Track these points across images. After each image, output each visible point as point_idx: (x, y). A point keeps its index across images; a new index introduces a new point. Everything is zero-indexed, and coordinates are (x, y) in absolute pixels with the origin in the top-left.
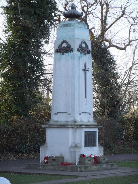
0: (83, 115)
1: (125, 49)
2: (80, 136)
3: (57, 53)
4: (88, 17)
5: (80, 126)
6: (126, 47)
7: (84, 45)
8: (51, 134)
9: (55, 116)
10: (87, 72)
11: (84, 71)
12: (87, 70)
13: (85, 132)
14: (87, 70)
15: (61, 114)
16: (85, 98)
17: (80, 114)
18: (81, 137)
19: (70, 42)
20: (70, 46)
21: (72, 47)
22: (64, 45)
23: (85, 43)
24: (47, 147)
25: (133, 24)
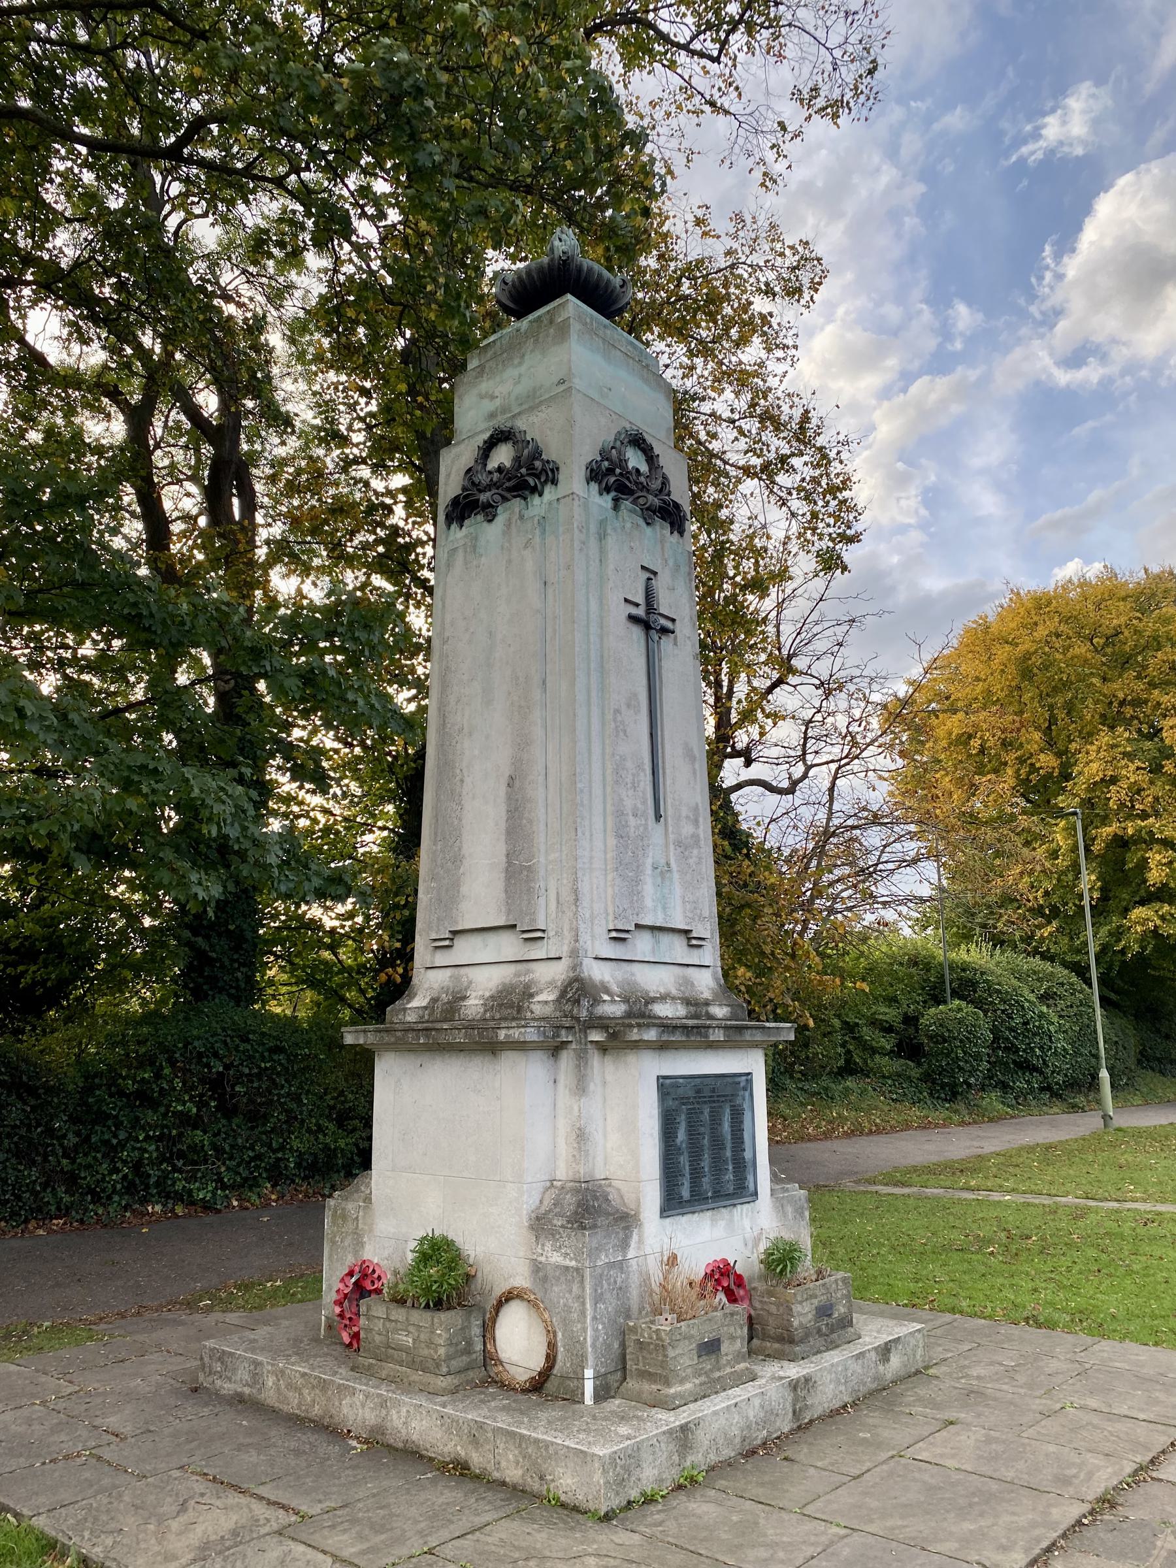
0: (642, 945)
1: (791, 791)
2: (619, 1122)
3: (454, 526)
4: (635, 1237)
5: (617, 1039)
6: (794, 784)
7: (635, 460)
8: (409, 1101)
9: (441, 959)
10: (666, 642)
11: (637, 632)
12: (664, 631)
13: (667, 1087)
14: (664, 631)
15: (476, 940)
16: (658, 817)
17: (619, 937)
18: (439, 786)
19: (531, 426)
20: (537, 454)
21: (552, 452)
22: (503, 456)
23: (638, 441)
24: (368, 1199)
25: (845, 627)
